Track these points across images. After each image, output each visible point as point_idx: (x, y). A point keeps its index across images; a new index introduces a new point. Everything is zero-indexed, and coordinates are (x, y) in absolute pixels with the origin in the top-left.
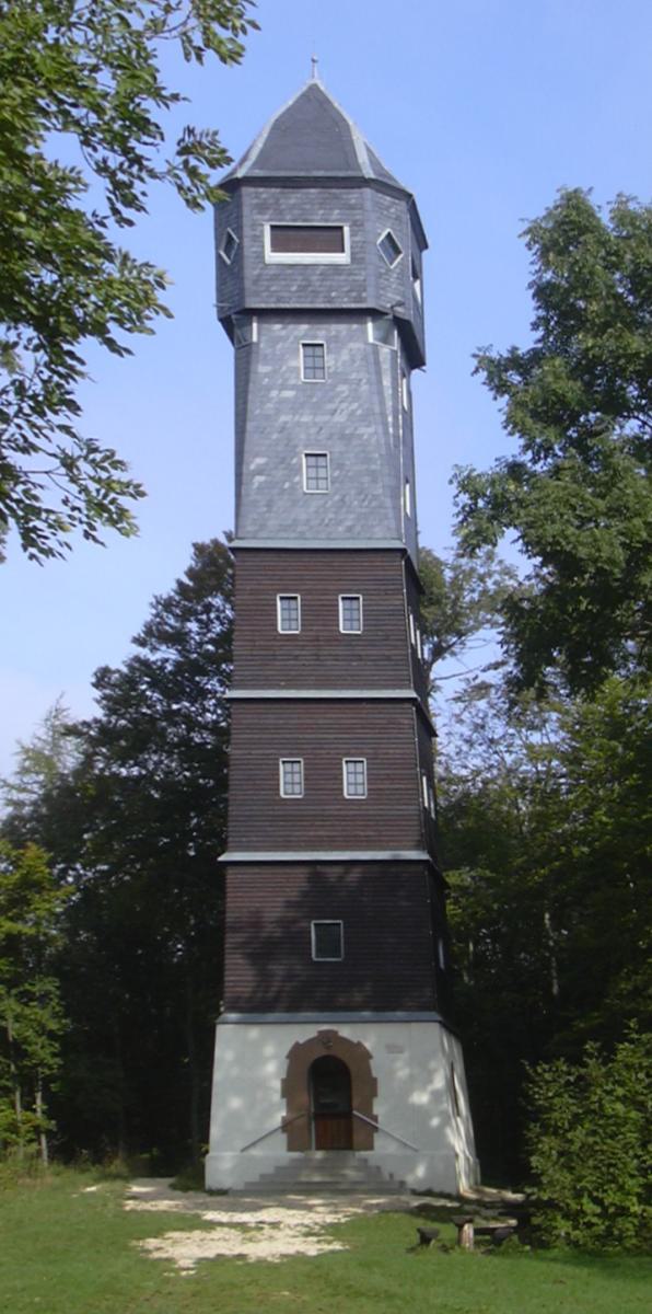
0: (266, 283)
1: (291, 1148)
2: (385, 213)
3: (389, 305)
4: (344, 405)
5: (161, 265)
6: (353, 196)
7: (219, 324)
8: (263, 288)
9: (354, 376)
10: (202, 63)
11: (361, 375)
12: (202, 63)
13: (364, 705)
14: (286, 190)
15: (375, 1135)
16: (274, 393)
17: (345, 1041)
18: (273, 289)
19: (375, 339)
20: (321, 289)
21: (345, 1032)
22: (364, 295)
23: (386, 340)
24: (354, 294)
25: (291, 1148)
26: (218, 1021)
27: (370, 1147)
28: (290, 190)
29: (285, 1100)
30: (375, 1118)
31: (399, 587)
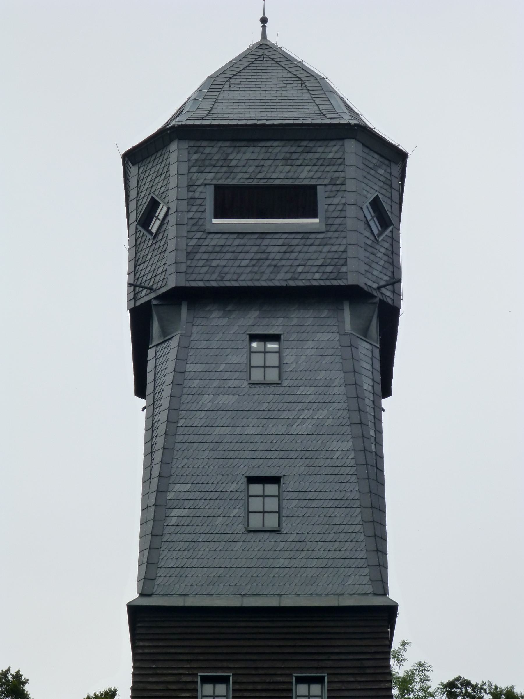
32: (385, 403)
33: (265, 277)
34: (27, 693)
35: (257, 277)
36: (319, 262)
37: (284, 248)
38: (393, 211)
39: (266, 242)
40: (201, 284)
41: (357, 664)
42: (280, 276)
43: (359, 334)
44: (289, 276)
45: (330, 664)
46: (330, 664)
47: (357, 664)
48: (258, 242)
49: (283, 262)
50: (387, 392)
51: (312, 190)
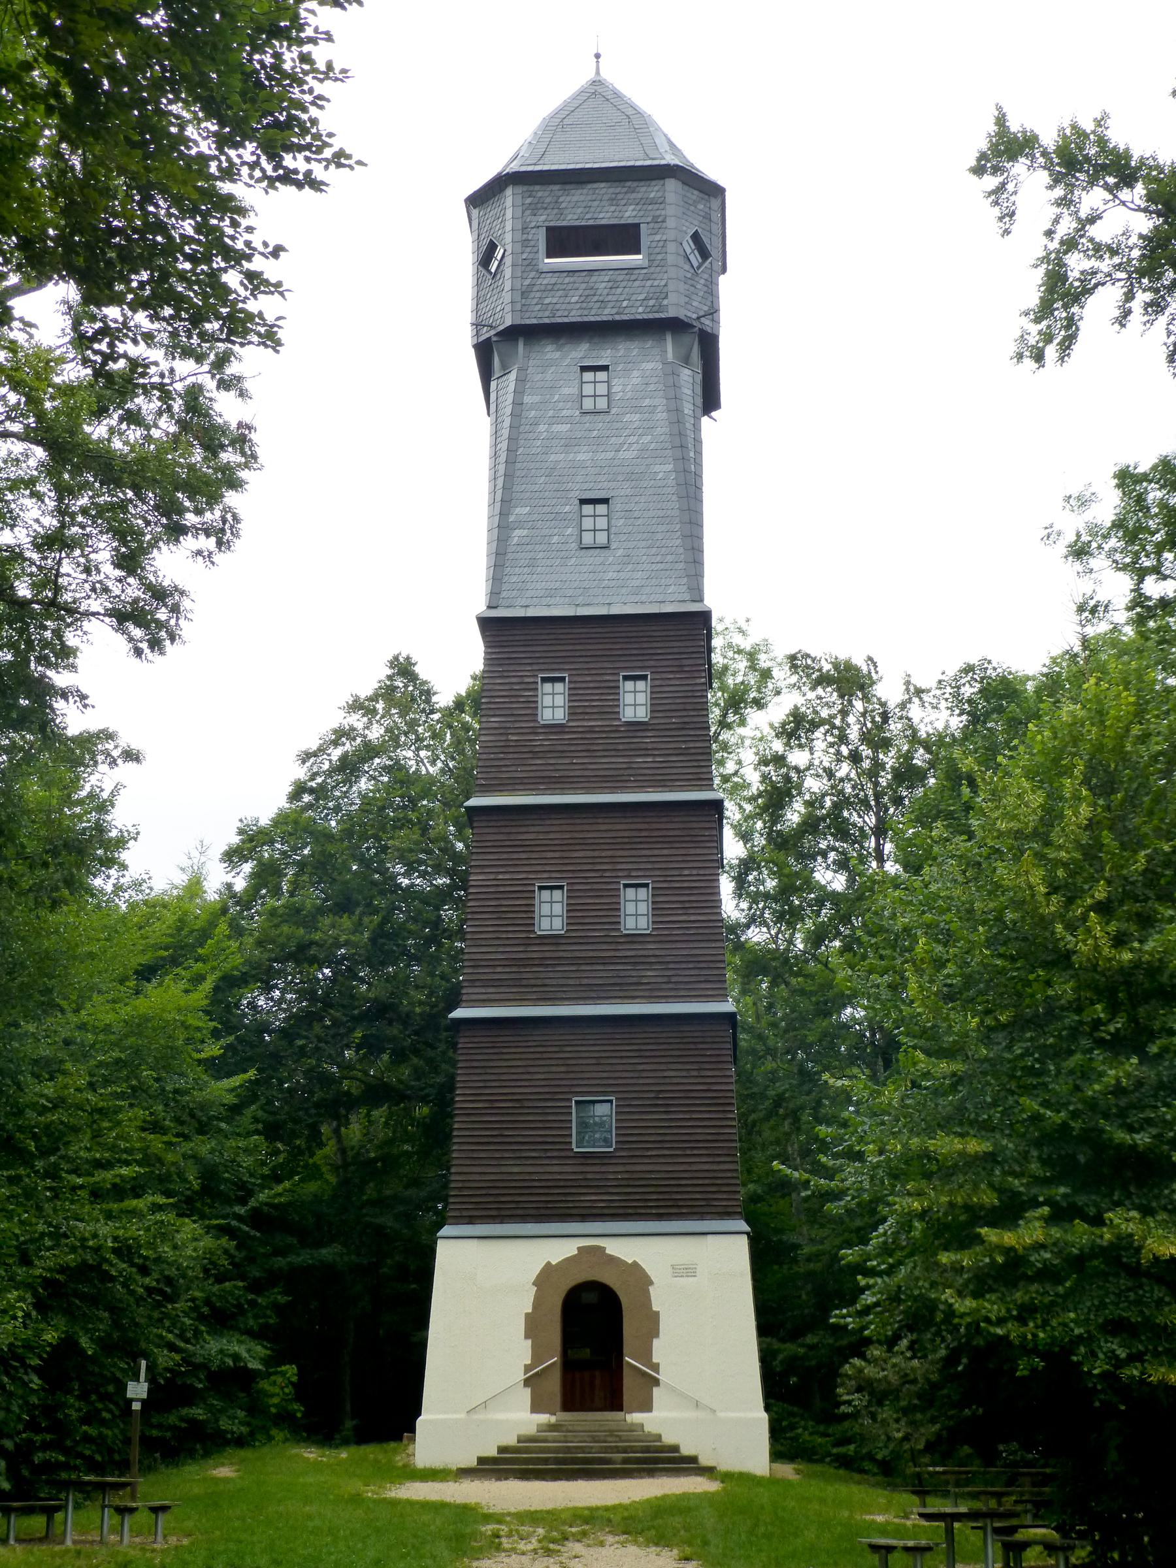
0: (538, 295)
1: (536, 1408)
2: (692, 208)
3: (695, 316)
4: (632, 439)
5: (237, 544)
6: (653, 190)
7: (473, 351)
8: (535, 301)
9: (647, 402)
10: (999, 108)
11: (657, 402)
12: (999, 108)
13: (709, 1237)
14: (568, 187)
15: (655, 1390)
16: (542, 428)
17: (613, 1260)
18: (547, 301)
19: (674, 357)
20: (610, 298)
21: (614, 1248)
22: (665, 302)
23: (686, 361)
24: (651, 303)
25: (536, 1408)
26: (439, 1234)
27: (647, 1406)
28: (572, 186)
29: (529, 1342)
30: (656, 1368)
31: (701, 662)
33: (593, 312)
35: (586, 312)
36: (642, 297)
37: (610, 284)
39: (594, 279)
42: (607, 311)
44: (614, 311)
45: (652, 663)
46: (652, 663)
48: (587, 279)
49: (610, 298)
50: (710, 400)
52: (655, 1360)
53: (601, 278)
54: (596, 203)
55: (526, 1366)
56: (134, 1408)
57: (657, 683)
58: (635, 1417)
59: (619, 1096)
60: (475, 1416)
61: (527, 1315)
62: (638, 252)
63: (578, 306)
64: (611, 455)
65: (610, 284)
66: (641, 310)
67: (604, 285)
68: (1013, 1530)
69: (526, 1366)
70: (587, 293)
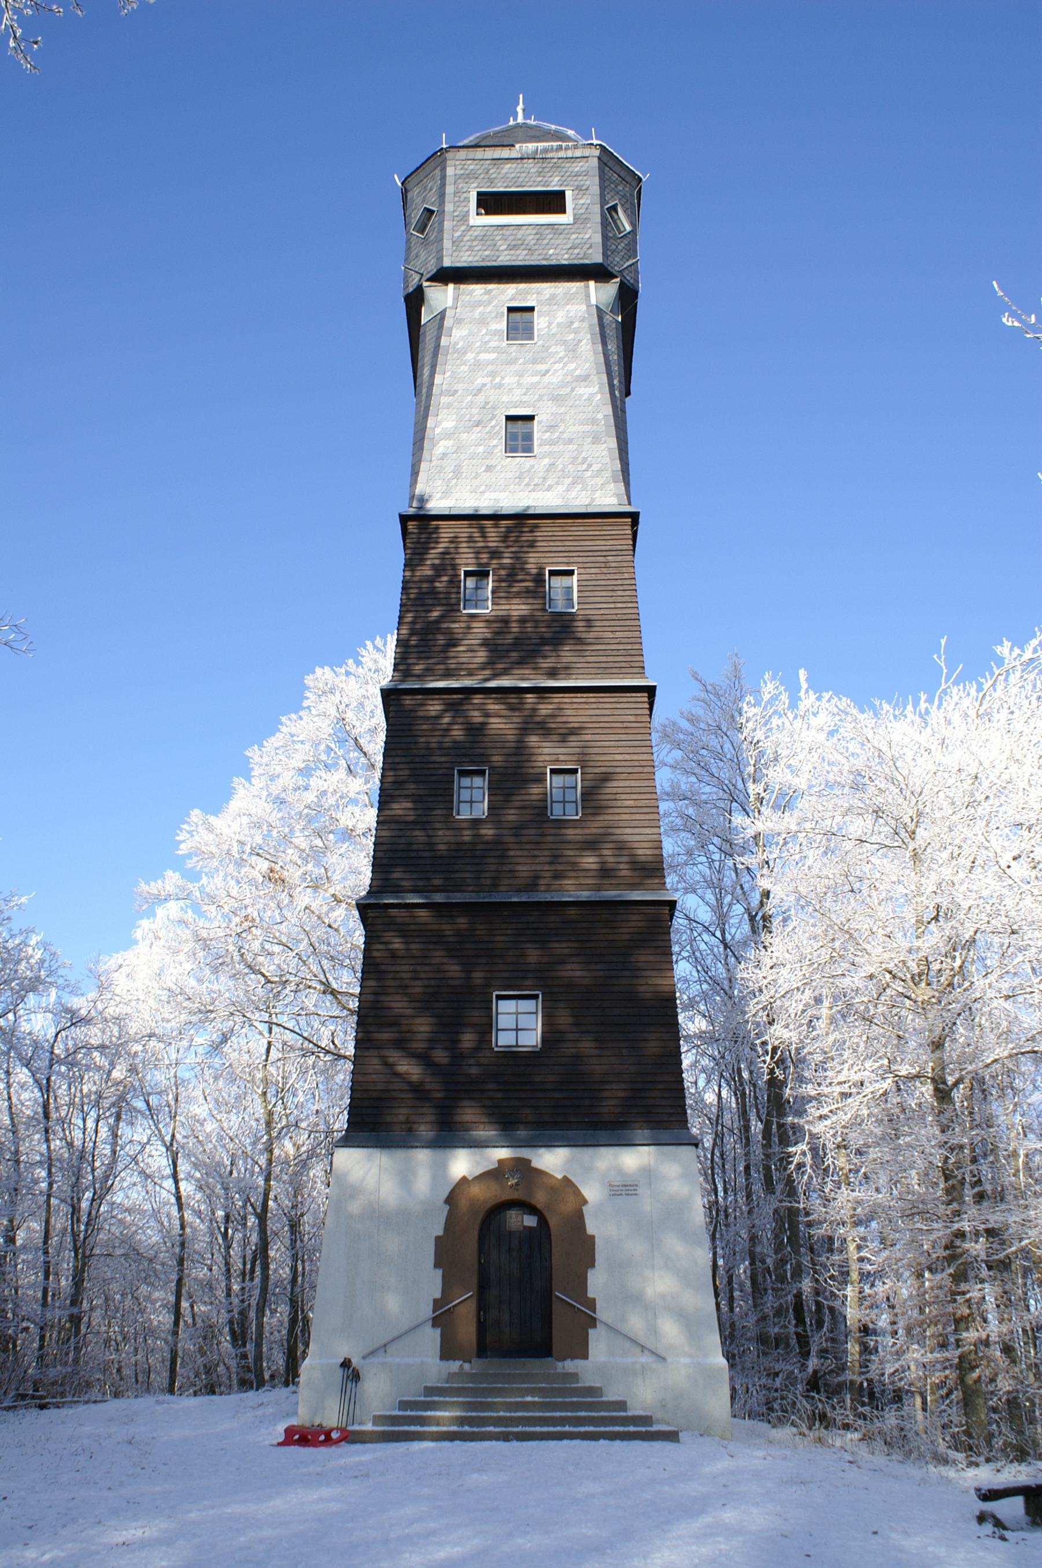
0: (469, 243)
4: (558, 366)
20: (537, 247)
32: (627, 399)
33: (520, 258)
34: (872, 707)
35: (514, 258)
36: (568, 246)
37: (537, 237)
38: (378, 1345)
39: (521, 232)
40: (465, 265)
41: (602, 559)
42: (533, 258)
43: (383, 1425)
44: (541, 257)
45: (580, 559)
46: (580, 559)
47: (602, 559)
48: (515, 232)
49: (537, 247)
50: (628, 393)
51: (561, 194)
52: (590, 1295)
53: (528, 232)
54: (524, 175)
55: (435, 1301)
56: (532, 1038)
57: (584, 577)
58: (571, 1366)
59: (580, 565)
60: (367, 1360)
61: (437, 1238)
62: (563, 211)
63: (507, 252)
64: (536, 379)
65: (537, 237)
66: (566, 256)
67: (531, 237)
68: (429, 879)
69: (435, 1301)
70: (514, 243)
